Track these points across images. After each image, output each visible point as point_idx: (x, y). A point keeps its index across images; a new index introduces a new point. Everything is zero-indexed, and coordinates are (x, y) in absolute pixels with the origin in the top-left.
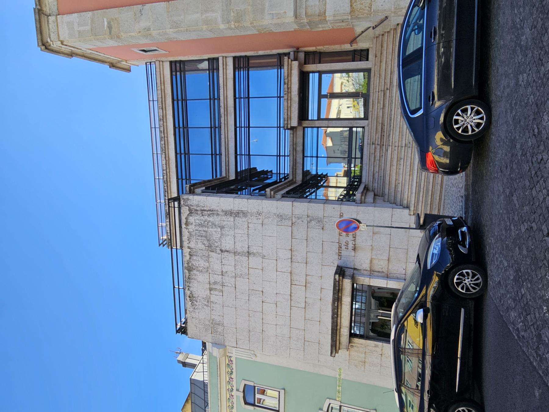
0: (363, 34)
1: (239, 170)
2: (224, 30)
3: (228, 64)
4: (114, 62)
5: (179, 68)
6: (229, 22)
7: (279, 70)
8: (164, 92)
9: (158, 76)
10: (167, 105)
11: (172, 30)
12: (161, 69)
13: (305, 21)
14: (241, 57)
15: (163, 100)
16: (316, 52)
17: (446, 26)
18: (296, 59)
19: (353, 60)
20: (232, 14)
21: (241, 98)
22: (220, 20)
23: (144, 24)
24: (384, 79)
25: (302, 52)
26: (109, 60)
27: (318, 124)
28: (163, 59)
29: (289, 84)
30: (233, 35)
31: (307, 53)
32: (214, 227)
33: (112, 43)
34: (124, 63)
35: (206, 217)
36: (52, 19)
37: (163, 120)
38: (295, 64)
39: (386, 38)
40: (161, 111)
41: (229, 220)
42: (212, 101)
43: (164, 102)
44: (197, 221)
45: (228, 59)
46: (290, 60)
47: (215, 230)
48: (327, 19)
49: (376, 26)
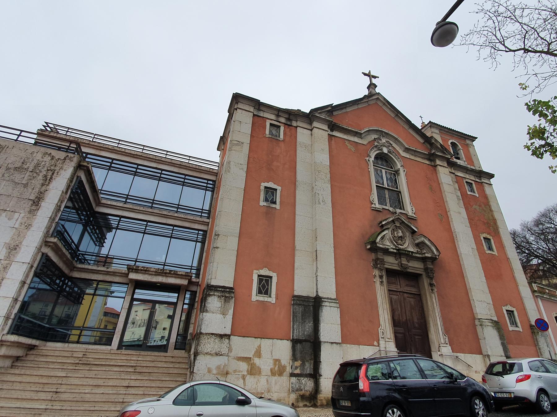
1: (110, 217)
27: (128, 298)
32: (29, 178)
35: (45, 173)
41: (32, 194)
44: (43, 163)
47: (26, 178)
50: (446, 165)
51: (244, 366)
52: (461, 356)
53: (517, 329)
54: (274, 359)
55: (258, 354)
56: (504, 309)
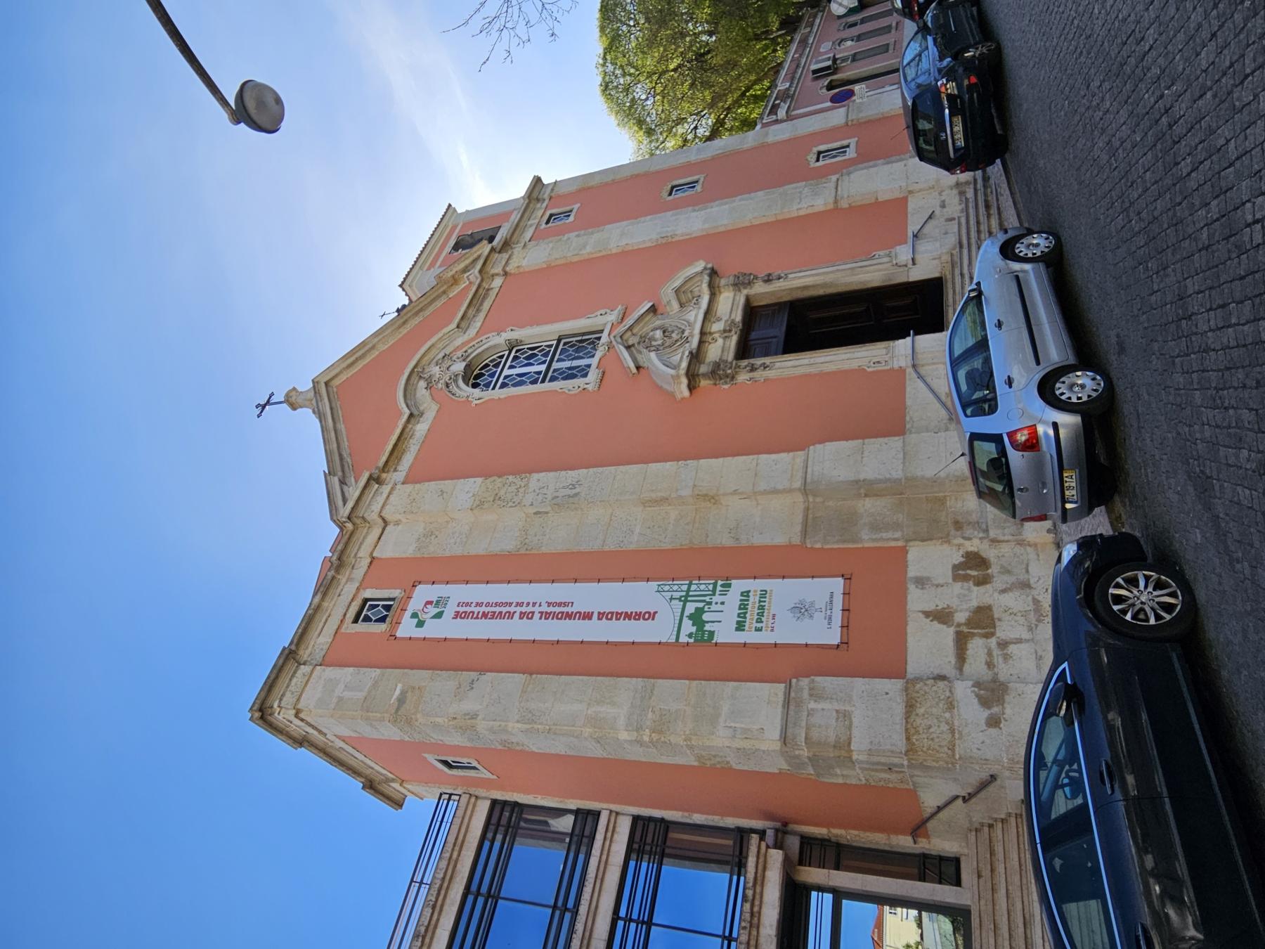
0: (941, 815)
2: (626, 745)
3: (618, 829)
4: (377, 778)
5: (508, 821)
6: (639, 729)
7: (735, 878)
8: (455, 866)
9: (455, 828)
10: (448, 901)
11: (519, 725)
12: (469, 812)
13: (805, 753)
14: (650, 819)
15: (445, 885)
16: (829, 841)
17: (1150, 839)
18: (778, 845)
19: (922, 878)
20: (650, 715)
21: (631, 920)
22: (622, 722)
23: (468, 706)
24: (1006, 935)
25: (794, 833)
26: (368, 772)
28: (481, 792)
29: (757, 903)
30: (644, 760)
31: (806, 841)
33: (390, 732)
34: (396, 785)
36: (304, 669)
37: (424, 938)
38: (776, 856)
39: (999, 832)
40: (428, 911)
42: (558, 912)
43: (443, 892)
45: (620, 818)
46: (763, 845)
48: (855, 757)
49: (971, 796)
50: (505, 256)
51: (977, 647)
52: (913, 228)
53: (853, 146)
54: (954, 580)
55: (942, 616)
56: (814, 164)
